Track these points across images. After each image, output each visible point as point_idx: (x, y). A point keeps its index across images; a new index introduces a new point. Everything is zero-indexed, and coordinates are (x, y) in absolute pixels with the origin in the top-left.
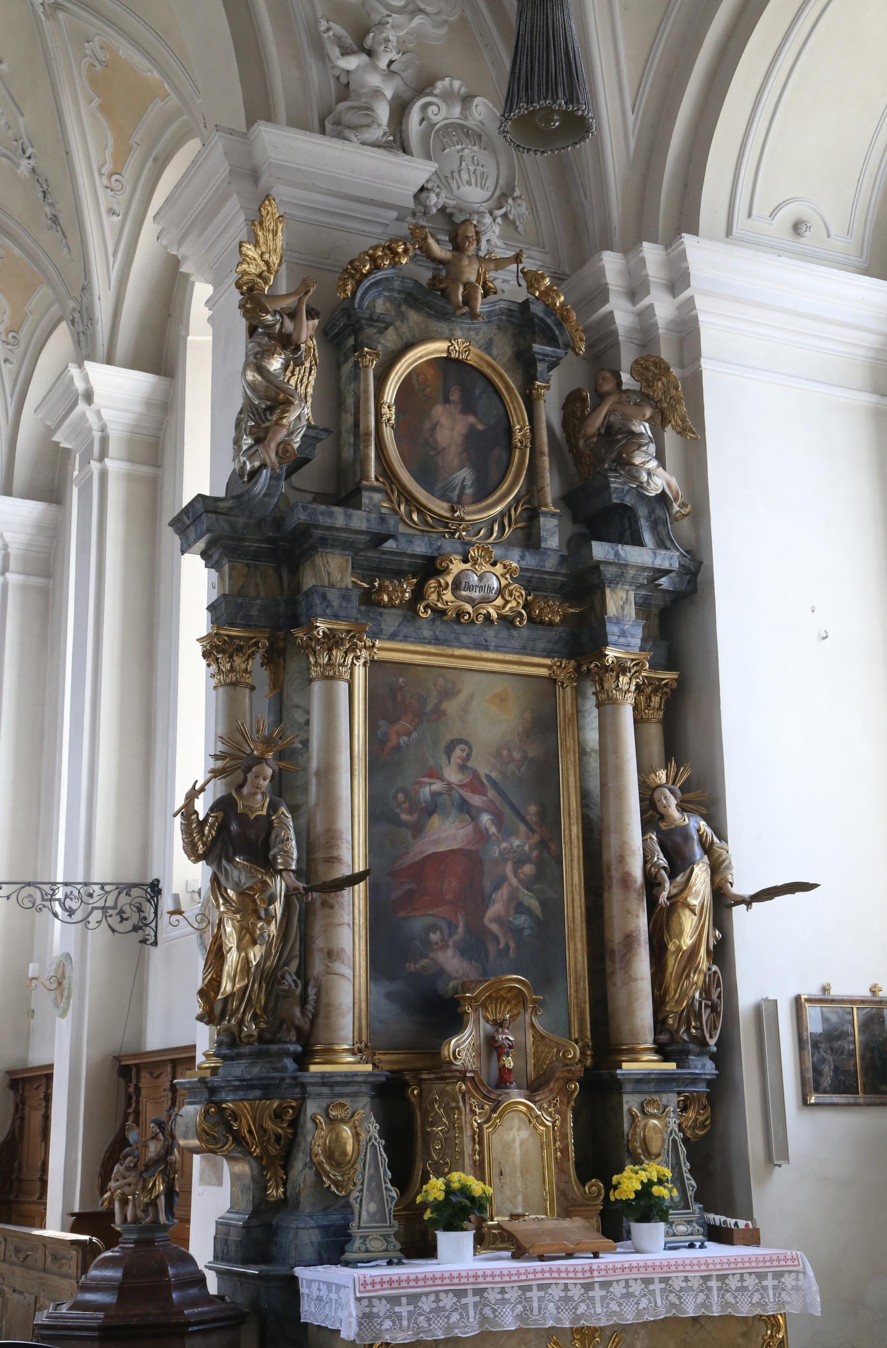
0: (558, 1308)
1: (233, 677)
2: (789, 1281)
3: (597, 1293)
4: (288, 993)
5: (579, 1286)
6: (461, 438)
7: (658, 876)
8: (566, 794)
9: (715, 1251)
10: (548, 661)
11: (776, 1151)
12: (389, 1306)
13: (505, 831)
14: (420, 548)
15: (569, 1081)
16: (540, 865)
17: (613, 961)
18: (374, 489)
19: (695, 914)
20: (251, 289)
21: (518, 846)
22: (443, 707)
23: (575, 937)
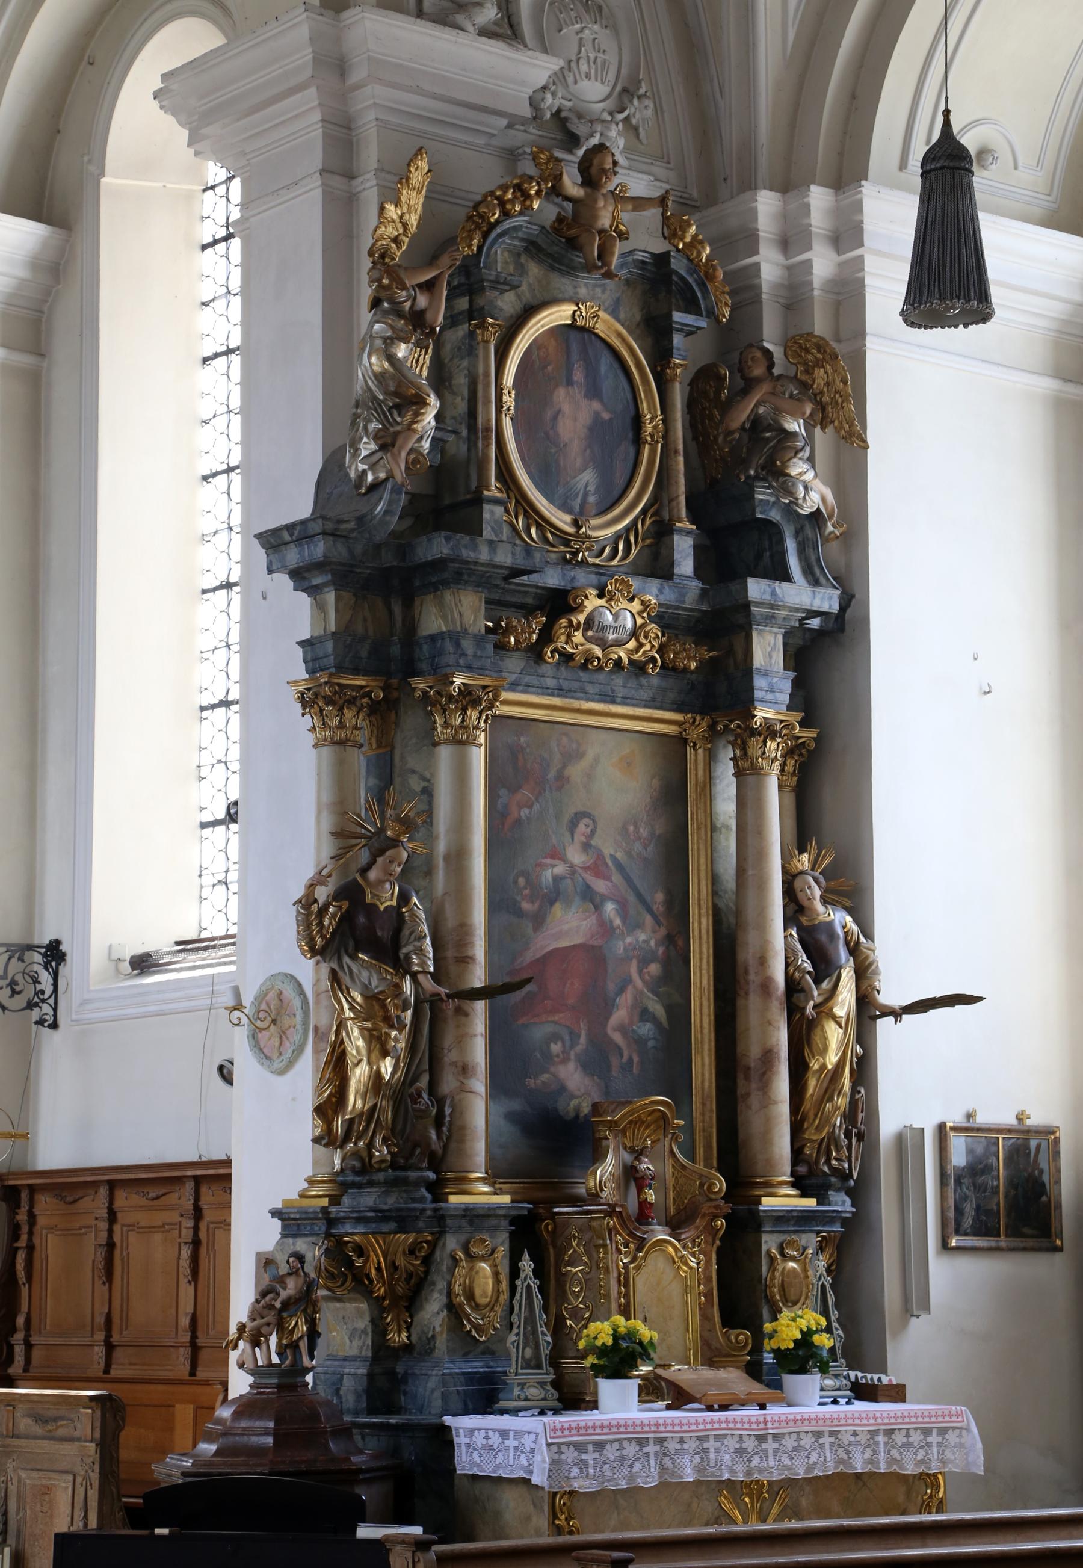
0: (733, 1460)
1: (341, 735)
2: (952, 1437)
3: (770, 1445)
4: (422, 1114)
5: (753, 1438)
6: (586, 430)
7: (802, 982)
8: (696, 881)
9: (860, 1406)
10: (679, 717)
11: (916, 1301)
12: (576, 1453)
13: (634, 926)
14: (552, 578)
15: (715, 1217)
16: (667, 964)
17: (747, 1078)
18: (496, 501)
19: (841, 1027)
20: (383, 256)
21: (644, 941)
22: (566, 773)
23: (702, 1049)
